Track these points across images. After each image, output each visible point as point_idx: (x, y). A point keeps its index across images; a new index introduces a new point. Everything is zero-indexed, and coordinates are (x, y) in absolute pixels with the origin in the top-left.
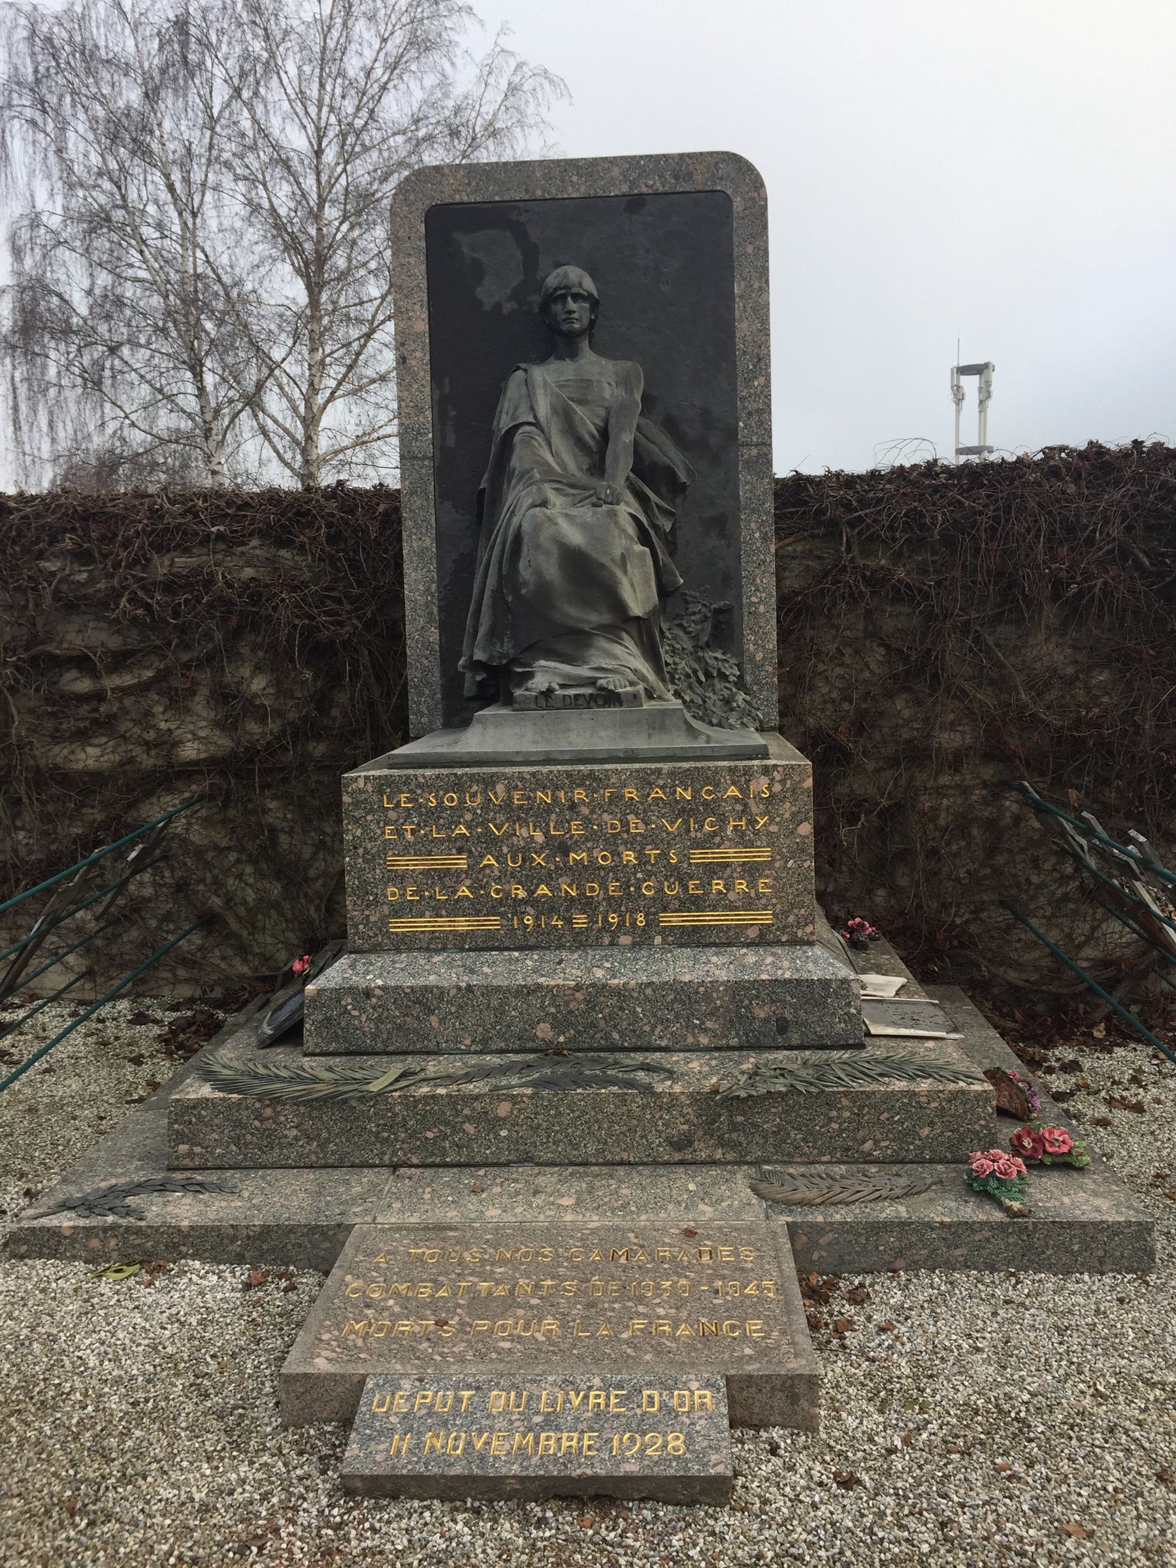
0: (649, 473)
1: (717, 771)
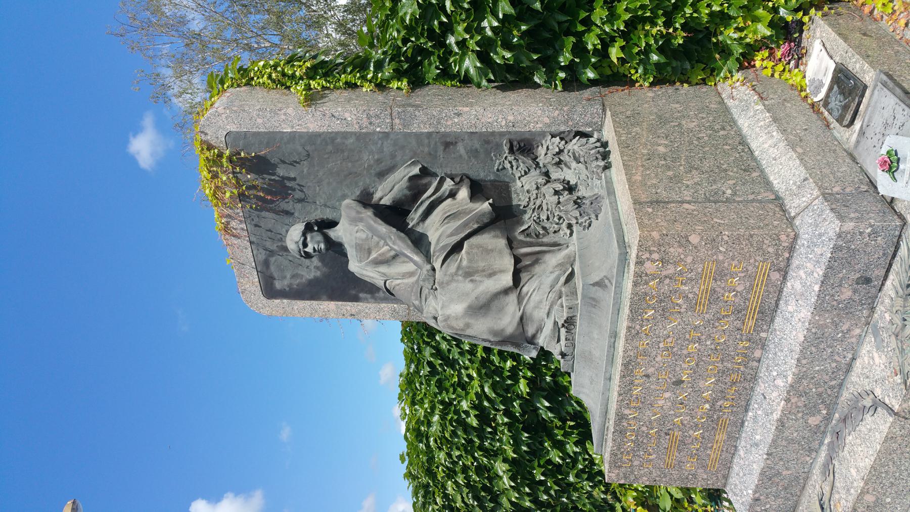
1: (635, 294)
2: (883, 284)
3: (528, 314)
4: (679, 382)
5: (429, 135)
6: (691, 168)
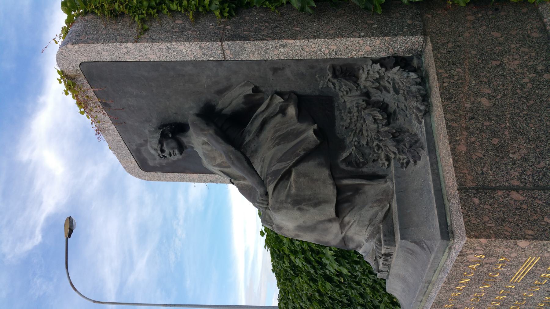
5: (258, 62)
6: (518, 133)
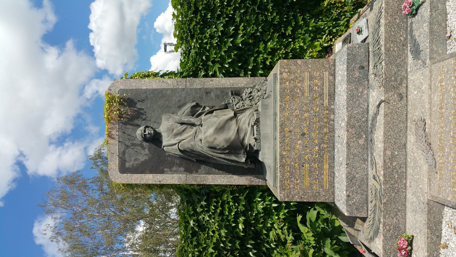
0: (195, 111)
1: (281, 88)
2: (369, 69)
3: (240, 128)
4: (304, 134)
5: (200, 89)
